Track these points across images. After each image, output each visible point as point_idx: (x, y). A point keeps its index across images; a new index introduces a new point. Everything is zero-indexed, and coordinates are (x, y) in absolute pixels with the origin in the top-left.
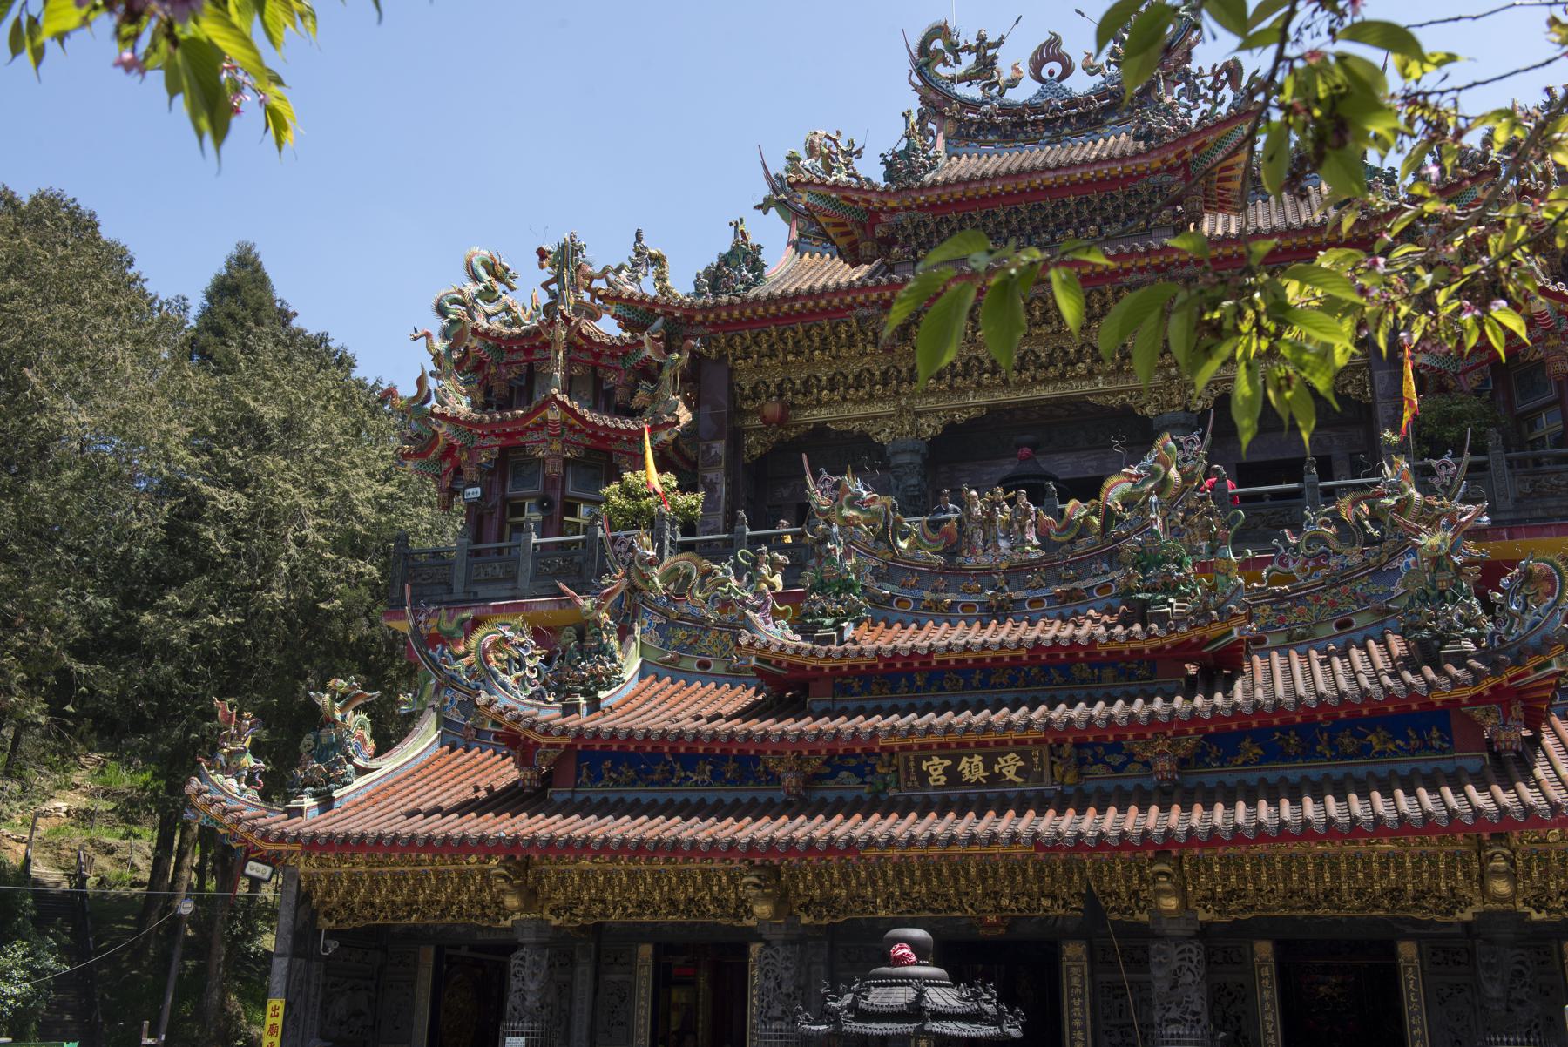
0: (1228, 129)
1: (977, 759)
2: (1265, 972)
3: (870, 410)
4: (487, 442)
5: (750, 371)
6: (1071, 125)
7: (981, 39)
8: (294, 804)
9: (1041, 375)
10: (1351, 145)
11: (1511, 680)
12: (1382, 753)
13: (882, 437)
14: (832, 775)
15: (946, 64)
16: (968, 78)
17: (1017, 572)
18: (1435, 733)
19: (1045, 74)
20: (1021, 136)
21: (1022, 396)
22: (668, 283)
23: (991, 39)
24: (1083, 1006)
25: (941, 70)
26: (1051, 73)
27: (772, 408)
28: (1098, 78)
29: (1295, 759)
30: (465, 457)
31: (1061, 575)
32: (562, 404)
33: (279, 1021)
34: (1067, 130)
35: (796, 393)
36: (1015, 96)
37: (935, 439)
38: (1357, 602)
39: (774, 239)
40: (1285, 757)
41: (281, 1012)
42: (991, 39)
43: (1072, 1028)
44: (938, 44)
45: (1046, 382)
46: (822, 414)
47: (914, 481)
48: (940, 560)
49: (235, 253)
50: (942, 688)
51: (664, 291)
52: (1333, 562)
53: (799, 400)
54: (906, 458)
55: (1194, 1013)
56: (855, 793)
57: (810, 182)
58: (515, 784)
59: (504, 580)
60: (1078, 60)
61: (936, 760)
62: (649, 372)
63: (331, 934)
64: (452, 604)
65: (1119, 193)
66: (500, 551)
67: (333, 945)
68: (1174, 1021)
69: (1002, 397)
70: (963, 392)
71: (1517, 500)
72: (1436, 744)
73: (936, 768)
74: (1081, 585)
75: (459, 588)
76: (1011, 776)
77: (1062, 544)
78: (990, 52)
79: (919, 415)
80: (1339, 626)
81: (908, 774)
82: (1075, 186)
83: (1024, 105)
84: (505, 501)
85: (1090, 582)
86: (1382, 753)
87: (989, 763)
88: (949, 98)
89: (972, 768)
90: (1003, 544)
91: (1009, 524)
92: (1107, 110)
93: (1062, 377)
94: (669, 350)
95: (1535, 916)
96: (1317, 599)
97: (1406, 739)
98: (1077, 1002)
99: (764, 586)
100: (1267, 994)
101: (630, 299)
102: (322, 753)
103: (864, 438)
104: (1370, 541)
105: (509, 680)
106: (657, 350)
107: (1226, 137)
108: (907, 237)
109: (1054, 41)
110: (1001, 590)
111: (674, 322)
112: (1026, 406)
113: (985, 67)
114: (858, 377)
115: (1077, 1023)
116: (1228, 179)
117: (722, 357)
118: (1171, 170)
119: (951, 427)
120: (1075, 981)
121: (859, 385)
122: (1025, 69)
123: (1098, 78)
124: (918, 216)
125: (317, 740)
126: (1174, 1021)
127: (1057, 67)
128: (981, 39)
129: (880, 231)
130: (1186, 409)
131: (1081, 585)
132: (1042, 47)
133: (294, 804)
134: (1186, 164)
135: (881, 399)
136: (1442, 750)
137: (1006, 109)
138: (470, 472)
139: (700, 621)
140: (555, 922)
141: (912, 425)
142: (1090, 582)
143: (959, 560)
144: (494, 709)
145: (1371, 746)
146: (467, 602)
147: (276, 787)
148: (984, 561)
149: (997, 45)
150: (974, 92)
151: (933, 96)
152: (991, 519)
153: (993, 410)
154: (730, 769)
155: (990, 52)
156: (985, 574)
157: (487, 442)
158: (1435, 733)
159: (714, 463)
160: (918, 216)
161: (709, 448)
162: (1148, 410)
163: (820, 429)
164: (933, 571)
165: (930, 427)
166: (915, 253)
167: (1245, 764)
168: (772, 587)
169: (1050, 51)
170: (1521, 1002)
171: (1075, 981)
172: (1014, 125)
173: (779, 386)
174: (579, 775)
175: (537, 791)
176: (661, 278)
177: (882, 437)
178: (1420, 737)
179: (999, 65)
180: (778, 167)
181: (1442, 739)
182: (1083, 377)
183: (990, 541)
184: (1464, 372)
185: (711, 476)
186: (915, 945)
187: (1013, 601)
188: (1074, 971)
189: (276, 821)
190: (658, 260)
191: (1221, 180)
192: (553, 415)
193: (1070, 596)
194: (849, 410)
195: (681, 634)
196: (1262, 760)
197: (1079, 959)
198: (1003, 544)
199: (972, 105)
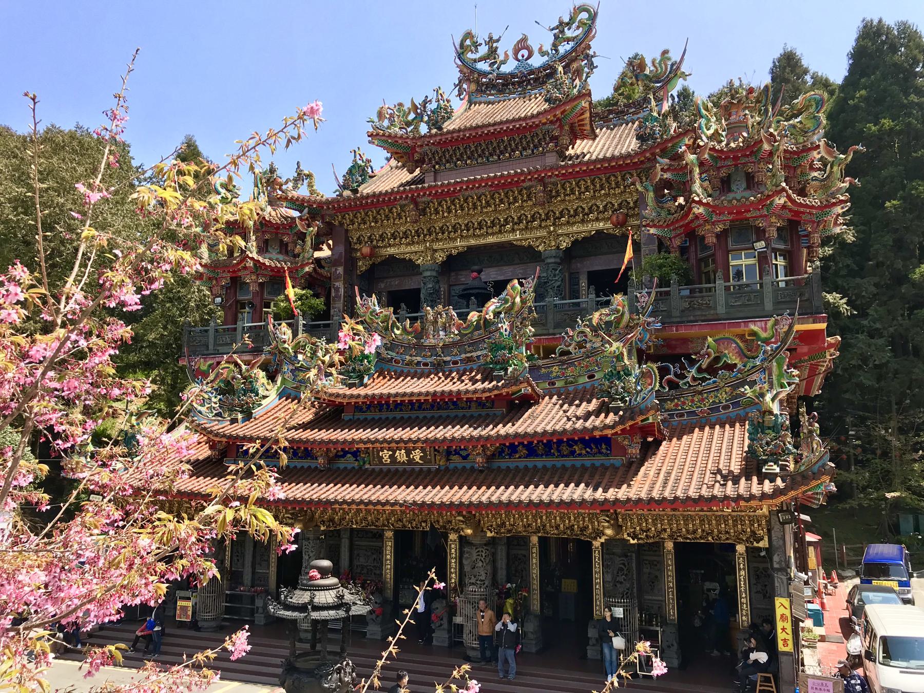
0: (576, 103)
1: (403, 451)
2: (534, 550)
3: (409, 249)
4: (224, 275)
5: (356, 230)
6: (531, 85)
7: (491, 38)
9: (490, 231)
11: (642, 421)
12: (580, 455)
13: (419, 262)
14: (343, 456)
18: (604, 446)
19: (520, 57)
20: (507, 91)
21: (482, 241)
22: (315, 188)
23: (495, 38)
24: (455, 562)
25: (470, 56)
26: (523, 56)
27: (366, 250)
28: (546, 58)
29: (542, 455)
34: (529, 87)
35: (378, 241)
36: (506, 69)
37: (443, 263)
38: (597, 365)
39: (378, 157)
40: (537, 456)
42: (495, 38)
43: (451, 573)
44: (468, 42)
45: (493, 234)
46: (391, 251)
47: (431, 286)
49: (185, 141)
50: (401, 410)
51: (312, 192)
52: (588, 345)
53: (380, 244)
55: (481, 581)
56: (352, 465)
57: (377, 134)
58: (208, 457)
60: (536, 49)
61: (386, 451)
62: (302, 236)
64: (206, 356)
68: (473, 584)
69: (473, 242)
70: (455, 239)
71: (683, 311)
72: (604, 451)
74: (474, 354)
75: (211, 347)
76: (418, 460)
77: (466, 334)
78: (495, 45)
79: (436, 251)
80: (589, 377)
81: (374, 458)
83: (509, 74)
84: (237, 302)
85: (479, 353)
86: (580, 455)
87: (408, 453)
88: (473, 71)
89: (401, 456)
90: (441, 333)
91: (444, 324)
93: (500, 232)
94: (309, 226)
95: (632, 542)
96: (580, 364)
97: (591, 449)
98: (453, 561)
99: (320, 362)
100: (534, 561)
101: (292, 199)
105: (203, 409)
106: (303, 226)
107: (576, 106)
108: (430, 160)
109: (524, 39)
110: (440, 356)
111: (314, 210)
112: (485, 246)
113: (493, 52)
115: (453, 570)
116: (583, 125)
117: (341, 224)
118: (552, 122)
119: (450, 257)
120: (453, 551)
122: (510, 53)
123: (546, 58)
124: (434, 149)
126: (473, 584)
127: (525, 52)
128: (491, 38)
130: (558, 247)
131: (474, 354)
132: (518, 42)
134: (558, 119)
136: (607, 455)
137: (499, 76)
141: (432, 256)
142: (479, 353)
143: (422, 341)
145: (575, 451)
149: (498, 41)
150: (483, 66)
151: (465, 70)
152: (435, 321)
153: (470, 248)
155: (495, 45)
156: (433, 348)
157: (224, 275)
158: (604, 446)
159: (338, 278)
160: (434, 149)
162: (540, 248)
163: (392, 257)
165: (440, 257)
166: (434, 167)
167: (520, 457)
169: (522, 44)
170: (621, 583)
171: (453, 551)
172: (503, 85)
175: (219, 460)
176: (310, 185)
177: (419, 262)
178: (597, 447)
179: (499, 51)
181: (607, 449)
182: (510, 232)
184: (675, 237)
185: (337, 284)
187: (445, 362)
188: (453, 546)
190: (309, 176)
191: (579, 125)
192: (250, 264)
194: (403, 249)
196: (527, 456)
197: (455, 541)
198: (441, 333)
199: (485, 74)
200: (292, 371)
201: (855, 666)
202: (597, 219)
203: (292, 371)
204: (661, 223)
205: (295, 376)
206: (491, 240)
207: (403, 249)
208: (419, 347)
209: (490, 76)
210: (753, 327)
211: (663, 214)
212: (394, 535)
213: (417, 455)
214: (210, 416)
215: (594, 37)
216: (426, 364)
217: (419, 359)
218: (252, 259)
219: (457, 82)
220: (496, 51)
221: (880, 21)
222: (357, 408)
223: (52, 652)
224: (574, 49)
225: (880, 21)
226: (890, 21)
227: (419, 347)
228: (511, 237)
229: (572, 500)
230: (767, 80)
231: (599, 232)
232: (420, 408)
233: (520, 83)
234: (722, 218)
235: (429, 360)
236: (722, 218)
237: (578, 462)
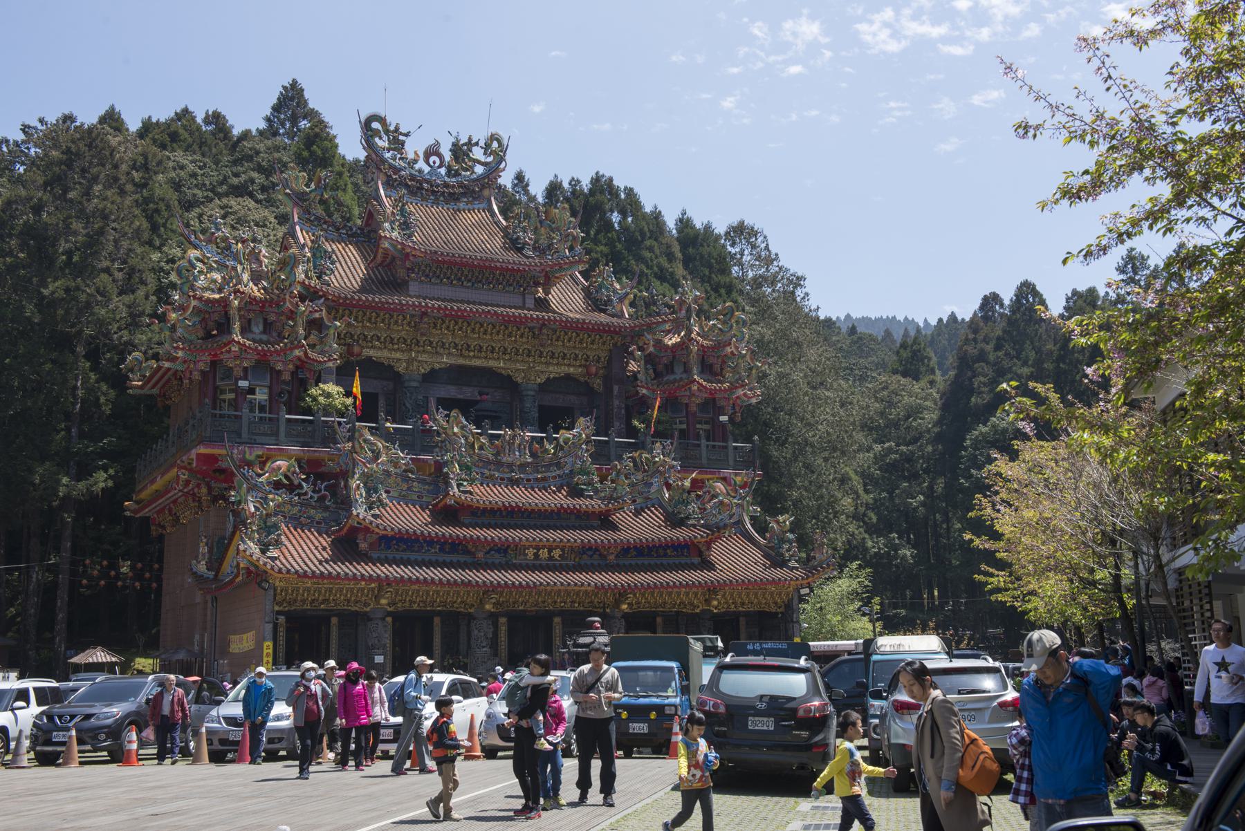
3: (398, 355)
10: (1085, 672)
15: (381, 138)
17: (523, 467)
21: (467, 362)
31: (538, 471)
46: (371, 353)
59: (271, 435)
66: (270, 419)
69: (461, 361)
73: (530, 553)
75: (245, 435)
78: (401, 138)
92: (464, 195)
103: (391, 367)
104: (645, 471)
122: (421, 155)
128: (397, 129)
149: (407, 135)
154: (447, 547)
156: (510, 466)
163: (369, 359)
164: (489, 462)
179: (406, 146)
183: (511, 451)
193: (544, 479)
194: (385, 354)
201: (1045, 696)
202: (569, 365)
206: (477, 363)
207: (385, 354)
213: (557, 553)
218: (238, 343)
223: (676, 743)
228: (491, 363)
230: (263, 125)
231: (568, 377)
232: (529, 517)
237: (671, 561)
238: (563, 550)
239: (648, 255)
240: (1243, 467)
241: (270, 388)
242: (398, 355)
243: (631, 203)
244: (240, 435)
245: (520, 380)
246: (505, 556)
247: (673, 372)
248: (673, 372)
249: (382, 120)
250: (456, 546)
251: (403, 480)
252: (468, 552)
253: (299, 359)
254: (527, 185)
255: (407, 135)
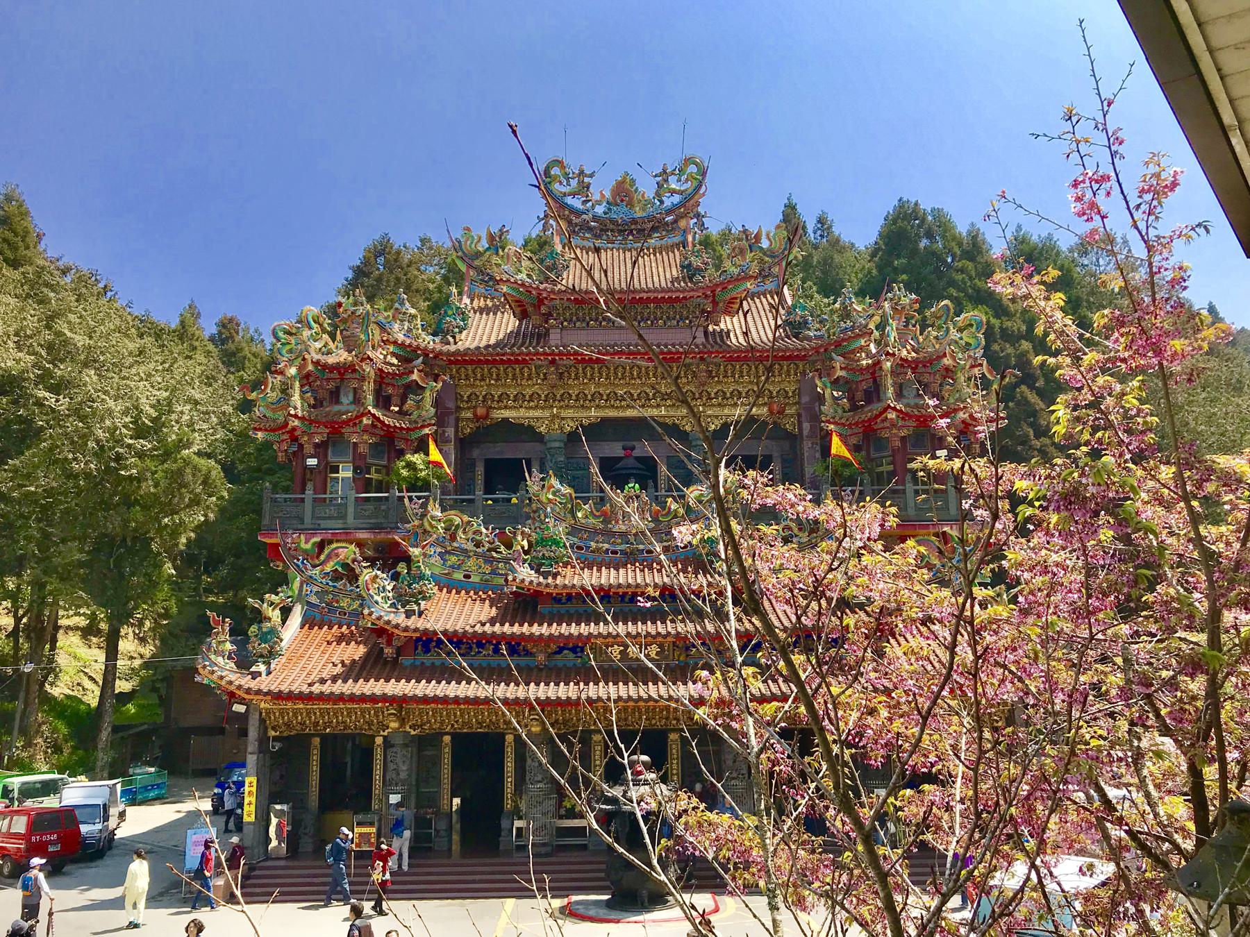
3: (532, 413)
8: (253, 669)
16: (574, 195)
21: (621, 414)
30: (306, 438)
32: (374, 415)
33: (254, 789)
41: (255, 784)
46: (506, 414)
48: (601, 526)
53: (495, 405)
54: (557, 444)
57: (508, 281)
63: (275, 739)
65: (678, 306)
67: (278, 745)
73: (615, 651)
78: (586, 180)
82: (655, 300)
92: (654, 229)
102: (264, 637)
103: (530, 428)
114: (531, 396)
121: (531, 400)
124: (567, 304)
125: (260, 628)
128: (582, 172)
129: (543, 310)
133: (253, 669)
135: (542, 408)
138: (308, 449)
139: (465, 551)
140: (413, 733)
144: (374, 616)
146: (316, 529)
147: (244, 663)
148: (623, 528)
149: (591, 176)
150: (576, 203)
153: (605, 421)
156: (623, 535)
161: (444, 432)
163: (505, 420)
164: (596, 532)
168: (523, 547)
172: (602, 230)
173: (484, 397)
174: (416, 648)
180: (458, 234)
186: (644, 763)
189: (247, 682)
194: (522, 413)
195: (453, 559)
199: (578, 213)
200: (440, 554)
203: (440, 554)
204: (843, 421)
205: (445, 560)
206: (630, 413)
208: (609, 534)
209: (584, 216)
210: (946, 529)
211: (840, 411)
212: (452, 741)
214: (386, 606)
215: (704, 194)
216: (615, 552)
217: (606, 546)
219: (542, 216)
220: (588, 188)
221: (916, 204)
222: (557, 599)
224: (682, 204)
225: (916, 204)
226: (926, 205)
227: (609, 534)
229: (548, 698)
233: (620, 231)
234: (907, 423)
235: (618, 548)
236: (907, 423)
238: (661, 646)
239: (959, 277)
240: (932, 934)
241: (353, 462)
242: (538, 413)
243: (942, 224)
244: (302, 520)
245: (688, 428)
246: (569, 660)
247: (338, 402)
248: (338, 402)
249: (559, 163)
250: (516, 645)
251: (486, 562)
252: (528, 653)
253: (963, 422)
254: (830, 227)
255: (591, 176)
